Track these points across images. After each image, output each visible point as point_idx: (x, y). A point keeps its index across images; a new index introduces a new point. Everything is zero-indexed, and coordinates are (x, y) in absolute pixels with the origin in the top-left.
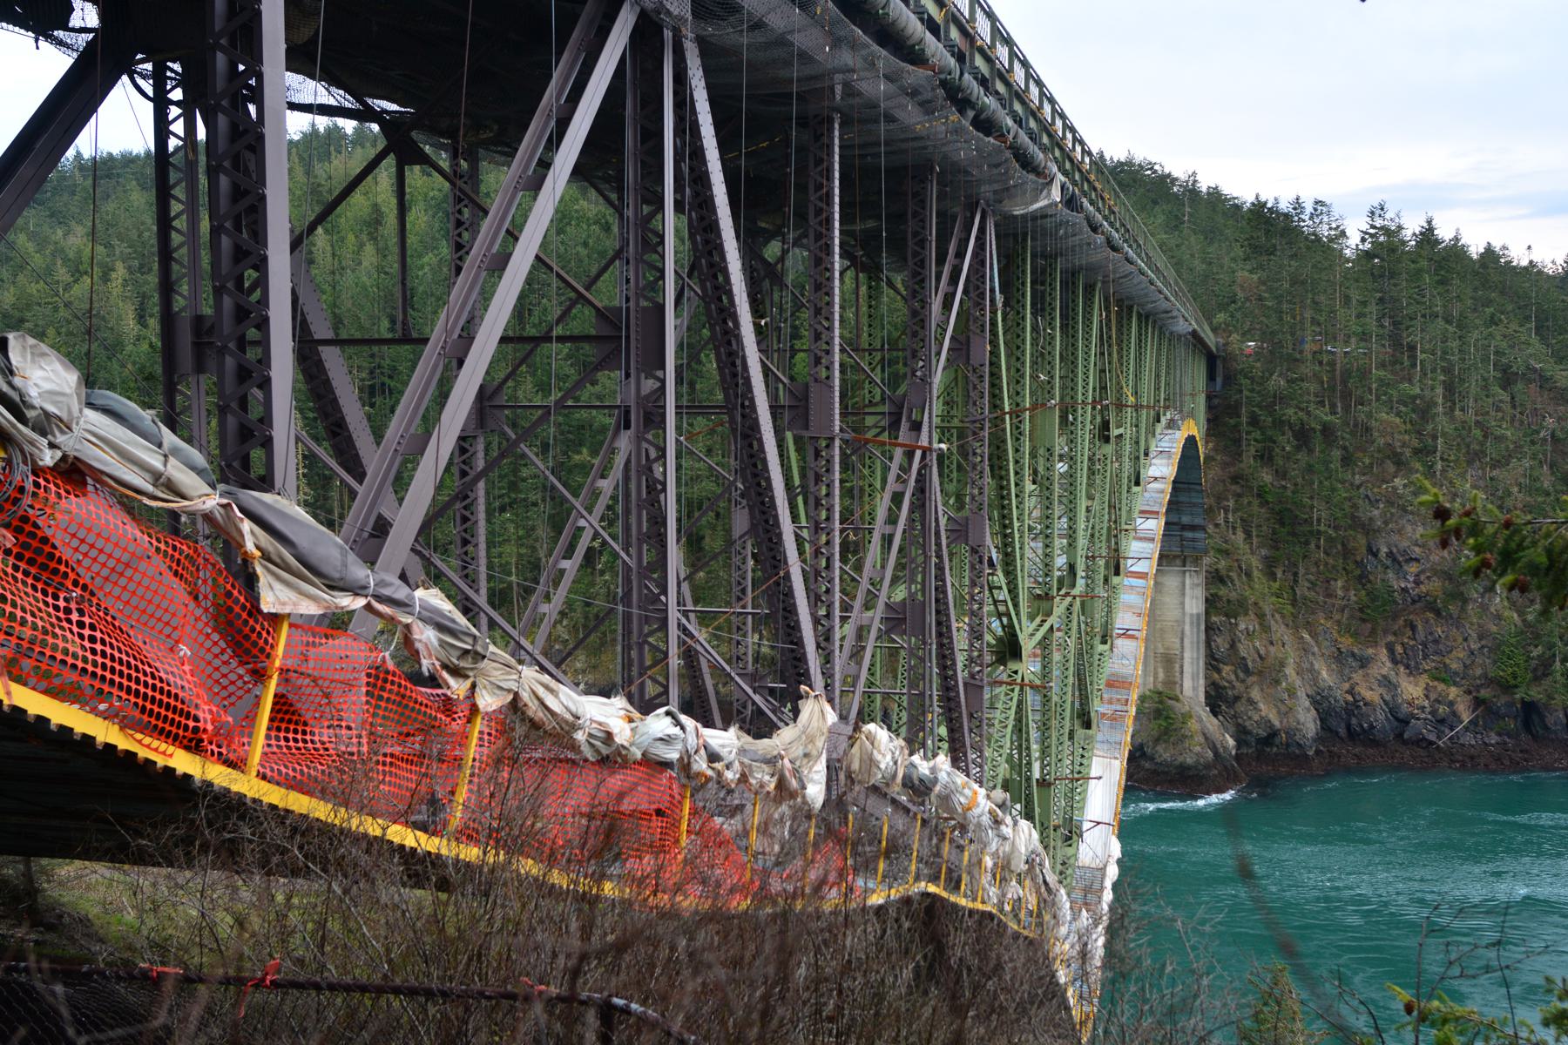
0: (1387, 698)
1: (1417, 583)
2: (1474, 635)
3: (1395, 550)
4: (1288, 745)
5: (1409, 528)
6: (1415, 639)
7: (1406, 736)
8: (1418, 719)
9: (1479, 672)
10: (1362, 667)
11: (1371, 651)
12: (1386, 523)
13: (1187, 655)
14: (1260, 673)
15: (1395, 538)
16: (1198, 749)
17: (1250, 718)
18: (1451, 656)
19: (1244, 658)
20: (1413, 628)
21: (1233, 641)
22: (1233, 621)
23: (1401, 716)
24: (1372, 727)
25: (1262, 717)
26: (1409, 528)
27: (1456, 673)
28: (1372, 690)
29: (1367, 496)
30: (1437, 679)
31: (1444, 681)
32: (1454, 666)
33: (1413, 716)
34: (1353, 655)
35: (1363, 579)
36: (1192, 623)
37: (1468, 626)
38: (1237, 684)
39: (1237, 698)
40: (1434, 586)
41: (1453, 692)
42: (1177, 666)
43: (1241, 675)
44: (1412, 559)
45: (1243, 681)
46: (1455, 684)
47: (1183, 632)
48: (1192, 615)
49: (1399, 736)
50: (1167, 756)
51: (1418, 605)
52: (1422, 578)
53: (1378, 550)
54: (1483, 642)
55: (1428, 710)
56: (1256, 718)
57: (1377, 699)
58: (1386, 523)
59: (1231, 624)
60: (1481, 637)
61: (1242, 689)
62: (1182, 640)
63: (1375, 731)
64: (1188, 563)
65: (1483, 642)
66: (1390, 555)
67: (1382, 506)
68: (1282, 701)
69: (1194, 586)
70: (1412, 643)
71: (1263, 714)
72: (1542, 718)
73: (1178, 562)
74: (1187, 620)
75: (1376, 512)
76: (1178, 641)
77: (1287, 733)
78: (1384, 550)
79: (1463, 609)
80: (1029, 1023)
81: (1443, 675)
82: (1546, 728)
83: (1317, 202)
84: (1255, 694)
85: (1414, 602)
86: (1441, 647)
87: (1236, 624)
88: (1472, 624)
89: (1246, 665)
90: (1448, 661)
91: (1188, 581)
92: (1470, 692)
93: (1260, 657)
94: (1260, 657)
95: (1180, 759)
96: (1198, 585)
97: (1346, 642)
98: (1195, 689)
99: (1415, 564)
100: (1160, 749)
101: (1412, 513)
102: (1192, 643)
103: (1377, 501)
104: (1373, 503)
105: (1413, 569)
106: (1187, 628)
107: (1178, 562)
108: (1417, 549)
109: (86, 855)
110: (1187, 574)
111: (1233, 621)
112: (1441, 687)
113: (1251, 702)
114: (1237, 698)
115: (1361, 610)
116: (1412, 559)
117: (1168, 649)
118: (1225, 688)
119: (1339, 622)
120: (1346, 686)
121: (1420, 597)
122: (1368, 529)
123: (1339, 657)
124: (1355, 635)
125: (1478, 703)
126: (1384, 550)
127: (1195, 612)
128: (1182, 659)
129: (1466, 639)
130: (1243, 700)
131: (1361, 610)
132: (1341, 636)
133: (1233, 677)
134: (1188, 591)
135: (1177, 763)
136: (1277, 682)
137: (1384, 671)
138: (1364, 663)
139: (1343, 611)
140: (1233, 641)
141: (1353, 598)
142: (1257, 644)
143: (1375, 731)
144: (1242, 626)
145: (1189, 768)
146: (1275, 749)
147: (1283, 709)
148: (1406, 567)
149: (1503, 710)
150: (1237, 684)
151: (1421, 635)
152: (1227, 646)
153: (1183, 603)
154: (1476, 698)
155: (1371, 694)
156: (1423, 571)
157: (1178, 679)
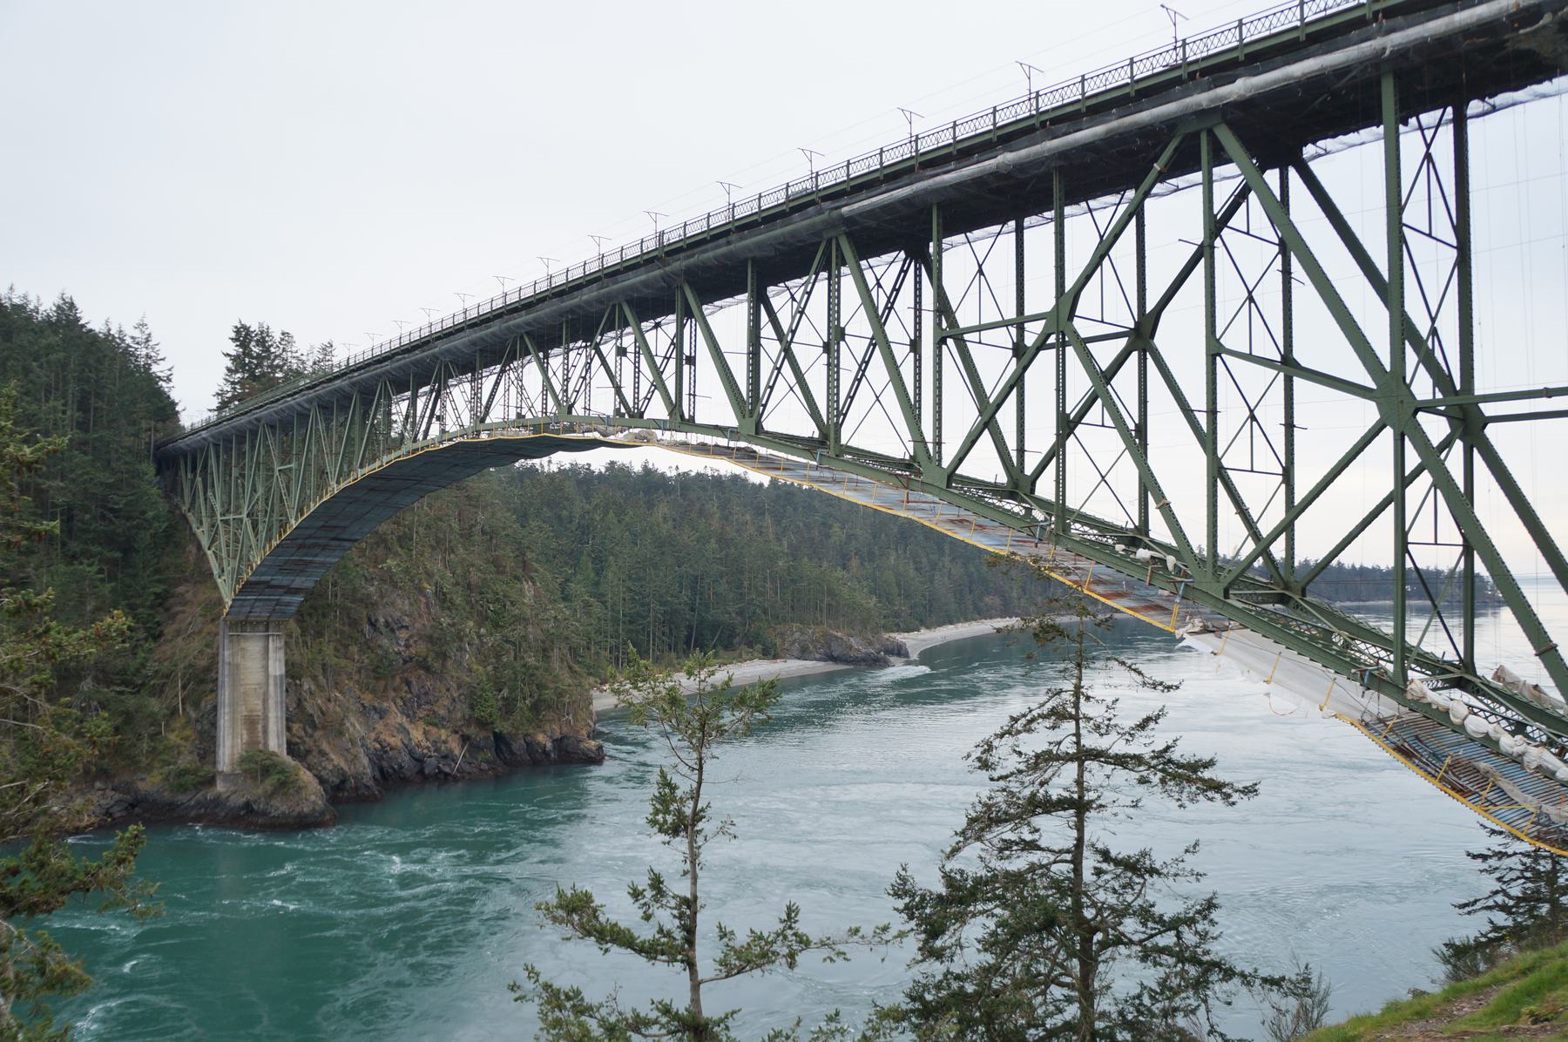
0: (406, 742)
1: (407, 646)
2: (455, 686)
3: (390, 620)
4: (356, 789)
5: (399, 601)
6: (411, 692)
7: (427, 771)
8: (430, 757)
9: (459, 715)
10: (381, 718)
11: (385, 704)
12: (382, 597)
13: (272, 715)
14: (324, 728)
15: (389, 609)
16: (313, 798)
17: (325, 768)
18: (438, 704)
19: (311, 715)
20: (408, 684)
21: (299, 700)
22: (298, 682)
23: (417, 756)
24: (401, 767)
25: (334, 765)
26: (399, 601)
27: (443, 718)
28: (394, 736)
29: (364, 576)
30: (430, 724)
31: (436, 725)
32: (442, 712)
33: (425, 755)
34: (375, 708)
35: (367, 646)
36: (276, 684)
37: (449, 678)
38: (307, 739)
39: (308, 752)
40: (421, 648)
41: (443, 734)
42: (260, 727)
43: (310, 731)
44: (402, 627)
45: (311, 736)
46: (443, 727)
47: (266, 694)
48: (275, 677)
49: (421, 771)
50: (284, 808)
51: (408, 665)
52: (411, 642)
53: (377, 620)
54: (461, 691)
55: (432, 749)
56: (330, 767)
57: (399, 744)
58: (382, 597)
59: (296, 685)
60: (459, 687)
61: (312, 743)
62: (265, 701)
63: (404, 770)
64: (271, 628)
65: (461, 691)
66: (387, 624)
67: (376, 583)
68: (348, 750)
69: (277, 649)
70: (409, 696)
71: (335, 763)
72: (508, 746)
73: (261, 627)
74: (271, 682)
75: (372, 589)
76: (260, 702)
77: (355, 778)
78: (382, 620)
79: (443, 666)
80: (892, 1029)
81: (433, 721)
82: (512, 753)
83: (283, 334)
84: (325, 746)
85: (405, 662)
86: (431, 697)
87: (301, 685)
88: (452, 677)
89: (313, 721)
90: (436, 709)
91: (271, 645)
92: (456, 732)
93: (323, 713)
94: (323, 713)
95: (298, 809)
96: (280, 648)
97: (367, 698)
98: (279, 746)
99: (403, 630)
100: (276, 802)
101: (401, 588)
102: (276, 703)
103: (372, 579)
104: (369, 580)
105: (403, 634)
106: (271, 688)
107: (261, 627)
108: (406, 618)
109: (1325, 138)
110: (271, 639)
111: (298, 682)
112: (434, 730)
113: (323, 753)
114: (308, 752)
115: (374, 671)
116: (402, 627)
117: (251, 711)
118: (297, 744)
119: (357, 682)
120: (373, 735)
121: (411, 659)
122: (367, 602)
123: (365, 711)
124: (373, 692)
125: (465, 739)
126: (382, 620)
127: (278, 673)
128: (266, 718)
129: (448, 690)
130: (315, 753)
131: (374, 671)
132: (363, 693)
133: (303, 733)
134: (271, 654)
135: (295, 814)
136: (341, 734)
137: (399, 720)
138: (382, 714)
139: (360, 672)
140: (299, 700)
141: (366, 661)
142: (319, 701)
143: (404, 770)
144: (306, 687)
145: (306, 816)
146: (346, 794)
147: (350, 757)
148: (397, 633)
149: (482, 743)
150: (307, 739)
151: (415, 689)
152: (295, 706)
153: (266, 668)
154: (462, 736)
155: (395, 741)
156: (411, 637)
157: (261, 739)
